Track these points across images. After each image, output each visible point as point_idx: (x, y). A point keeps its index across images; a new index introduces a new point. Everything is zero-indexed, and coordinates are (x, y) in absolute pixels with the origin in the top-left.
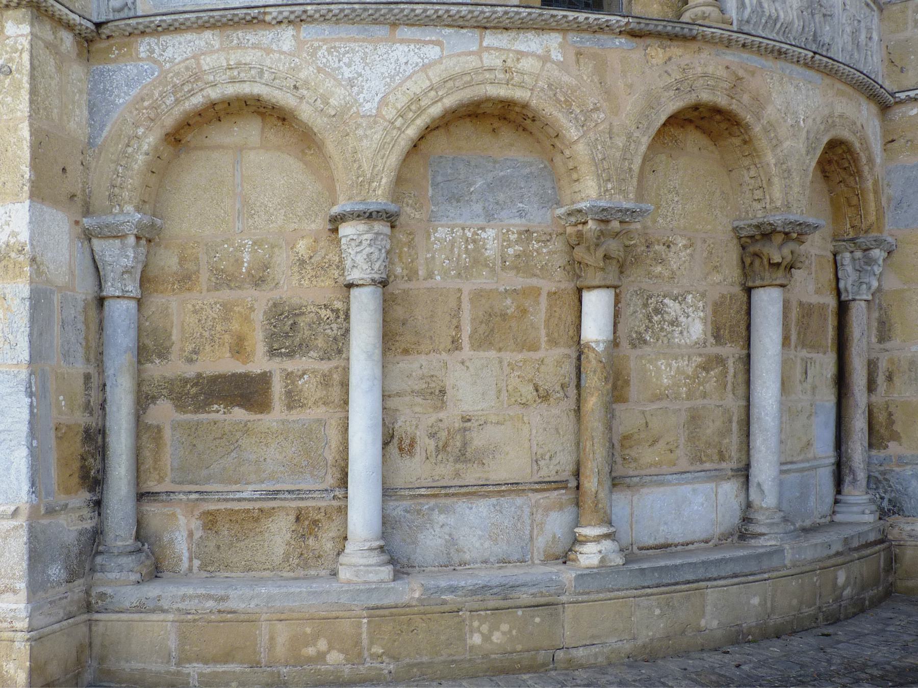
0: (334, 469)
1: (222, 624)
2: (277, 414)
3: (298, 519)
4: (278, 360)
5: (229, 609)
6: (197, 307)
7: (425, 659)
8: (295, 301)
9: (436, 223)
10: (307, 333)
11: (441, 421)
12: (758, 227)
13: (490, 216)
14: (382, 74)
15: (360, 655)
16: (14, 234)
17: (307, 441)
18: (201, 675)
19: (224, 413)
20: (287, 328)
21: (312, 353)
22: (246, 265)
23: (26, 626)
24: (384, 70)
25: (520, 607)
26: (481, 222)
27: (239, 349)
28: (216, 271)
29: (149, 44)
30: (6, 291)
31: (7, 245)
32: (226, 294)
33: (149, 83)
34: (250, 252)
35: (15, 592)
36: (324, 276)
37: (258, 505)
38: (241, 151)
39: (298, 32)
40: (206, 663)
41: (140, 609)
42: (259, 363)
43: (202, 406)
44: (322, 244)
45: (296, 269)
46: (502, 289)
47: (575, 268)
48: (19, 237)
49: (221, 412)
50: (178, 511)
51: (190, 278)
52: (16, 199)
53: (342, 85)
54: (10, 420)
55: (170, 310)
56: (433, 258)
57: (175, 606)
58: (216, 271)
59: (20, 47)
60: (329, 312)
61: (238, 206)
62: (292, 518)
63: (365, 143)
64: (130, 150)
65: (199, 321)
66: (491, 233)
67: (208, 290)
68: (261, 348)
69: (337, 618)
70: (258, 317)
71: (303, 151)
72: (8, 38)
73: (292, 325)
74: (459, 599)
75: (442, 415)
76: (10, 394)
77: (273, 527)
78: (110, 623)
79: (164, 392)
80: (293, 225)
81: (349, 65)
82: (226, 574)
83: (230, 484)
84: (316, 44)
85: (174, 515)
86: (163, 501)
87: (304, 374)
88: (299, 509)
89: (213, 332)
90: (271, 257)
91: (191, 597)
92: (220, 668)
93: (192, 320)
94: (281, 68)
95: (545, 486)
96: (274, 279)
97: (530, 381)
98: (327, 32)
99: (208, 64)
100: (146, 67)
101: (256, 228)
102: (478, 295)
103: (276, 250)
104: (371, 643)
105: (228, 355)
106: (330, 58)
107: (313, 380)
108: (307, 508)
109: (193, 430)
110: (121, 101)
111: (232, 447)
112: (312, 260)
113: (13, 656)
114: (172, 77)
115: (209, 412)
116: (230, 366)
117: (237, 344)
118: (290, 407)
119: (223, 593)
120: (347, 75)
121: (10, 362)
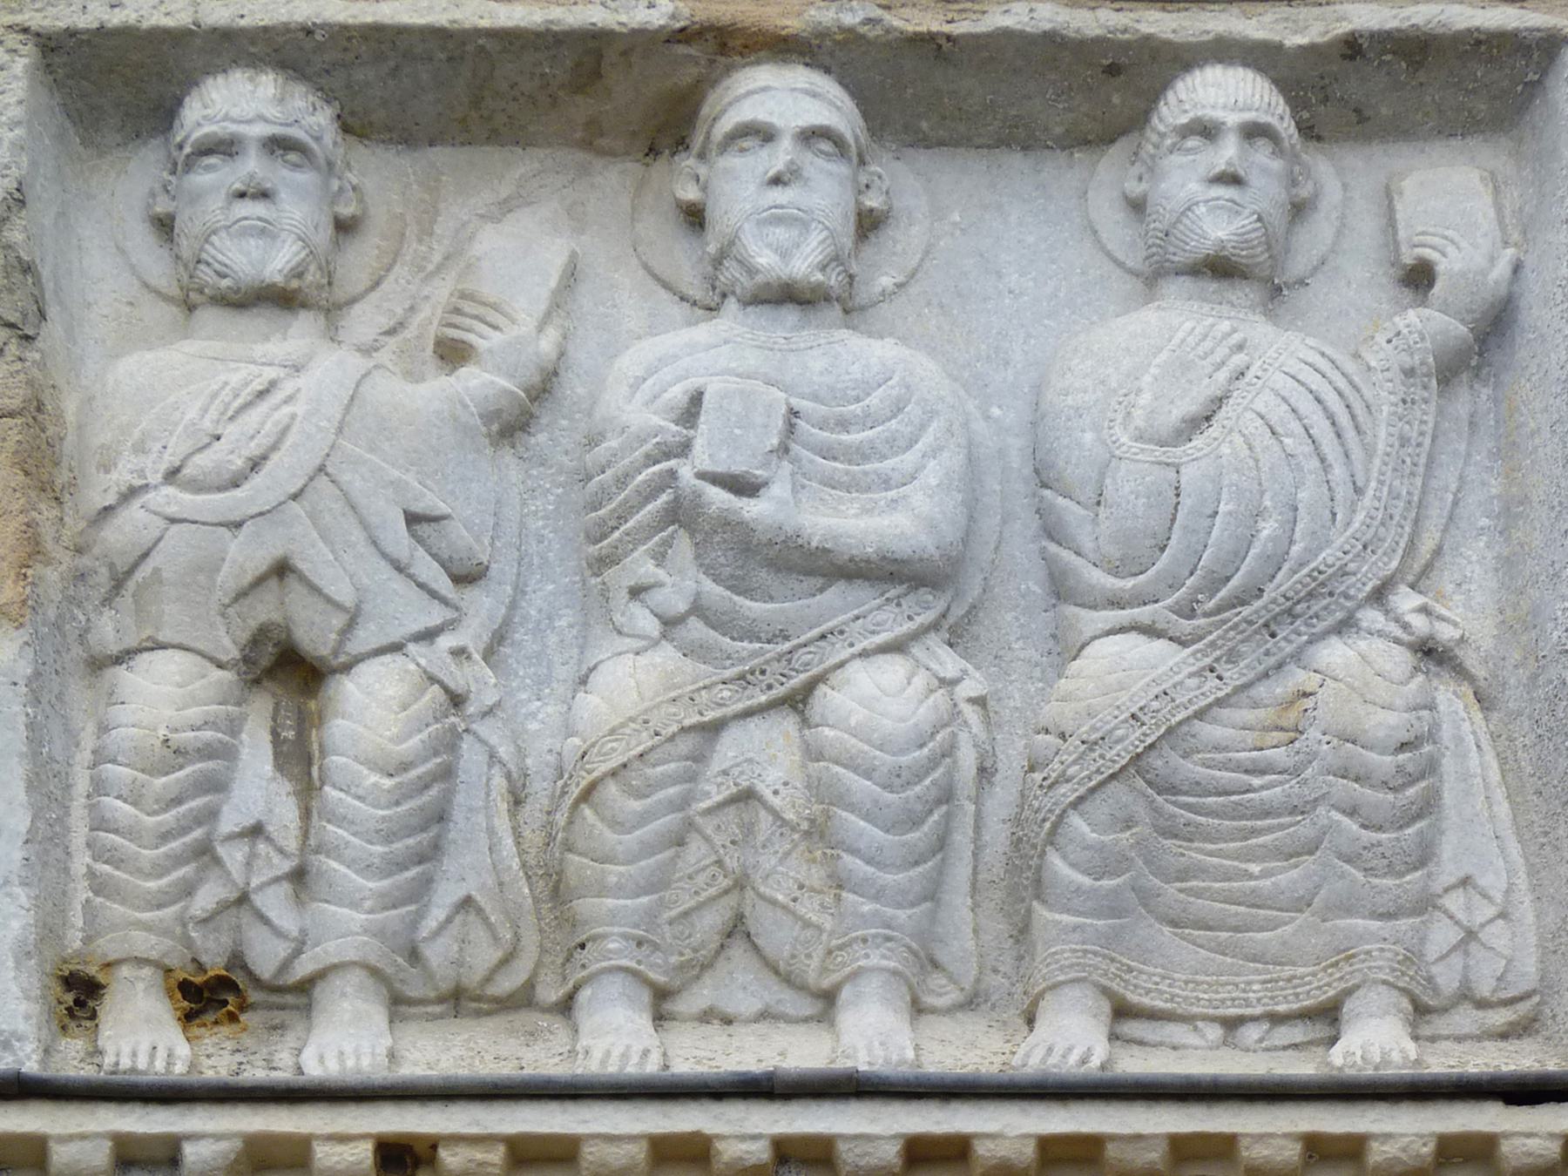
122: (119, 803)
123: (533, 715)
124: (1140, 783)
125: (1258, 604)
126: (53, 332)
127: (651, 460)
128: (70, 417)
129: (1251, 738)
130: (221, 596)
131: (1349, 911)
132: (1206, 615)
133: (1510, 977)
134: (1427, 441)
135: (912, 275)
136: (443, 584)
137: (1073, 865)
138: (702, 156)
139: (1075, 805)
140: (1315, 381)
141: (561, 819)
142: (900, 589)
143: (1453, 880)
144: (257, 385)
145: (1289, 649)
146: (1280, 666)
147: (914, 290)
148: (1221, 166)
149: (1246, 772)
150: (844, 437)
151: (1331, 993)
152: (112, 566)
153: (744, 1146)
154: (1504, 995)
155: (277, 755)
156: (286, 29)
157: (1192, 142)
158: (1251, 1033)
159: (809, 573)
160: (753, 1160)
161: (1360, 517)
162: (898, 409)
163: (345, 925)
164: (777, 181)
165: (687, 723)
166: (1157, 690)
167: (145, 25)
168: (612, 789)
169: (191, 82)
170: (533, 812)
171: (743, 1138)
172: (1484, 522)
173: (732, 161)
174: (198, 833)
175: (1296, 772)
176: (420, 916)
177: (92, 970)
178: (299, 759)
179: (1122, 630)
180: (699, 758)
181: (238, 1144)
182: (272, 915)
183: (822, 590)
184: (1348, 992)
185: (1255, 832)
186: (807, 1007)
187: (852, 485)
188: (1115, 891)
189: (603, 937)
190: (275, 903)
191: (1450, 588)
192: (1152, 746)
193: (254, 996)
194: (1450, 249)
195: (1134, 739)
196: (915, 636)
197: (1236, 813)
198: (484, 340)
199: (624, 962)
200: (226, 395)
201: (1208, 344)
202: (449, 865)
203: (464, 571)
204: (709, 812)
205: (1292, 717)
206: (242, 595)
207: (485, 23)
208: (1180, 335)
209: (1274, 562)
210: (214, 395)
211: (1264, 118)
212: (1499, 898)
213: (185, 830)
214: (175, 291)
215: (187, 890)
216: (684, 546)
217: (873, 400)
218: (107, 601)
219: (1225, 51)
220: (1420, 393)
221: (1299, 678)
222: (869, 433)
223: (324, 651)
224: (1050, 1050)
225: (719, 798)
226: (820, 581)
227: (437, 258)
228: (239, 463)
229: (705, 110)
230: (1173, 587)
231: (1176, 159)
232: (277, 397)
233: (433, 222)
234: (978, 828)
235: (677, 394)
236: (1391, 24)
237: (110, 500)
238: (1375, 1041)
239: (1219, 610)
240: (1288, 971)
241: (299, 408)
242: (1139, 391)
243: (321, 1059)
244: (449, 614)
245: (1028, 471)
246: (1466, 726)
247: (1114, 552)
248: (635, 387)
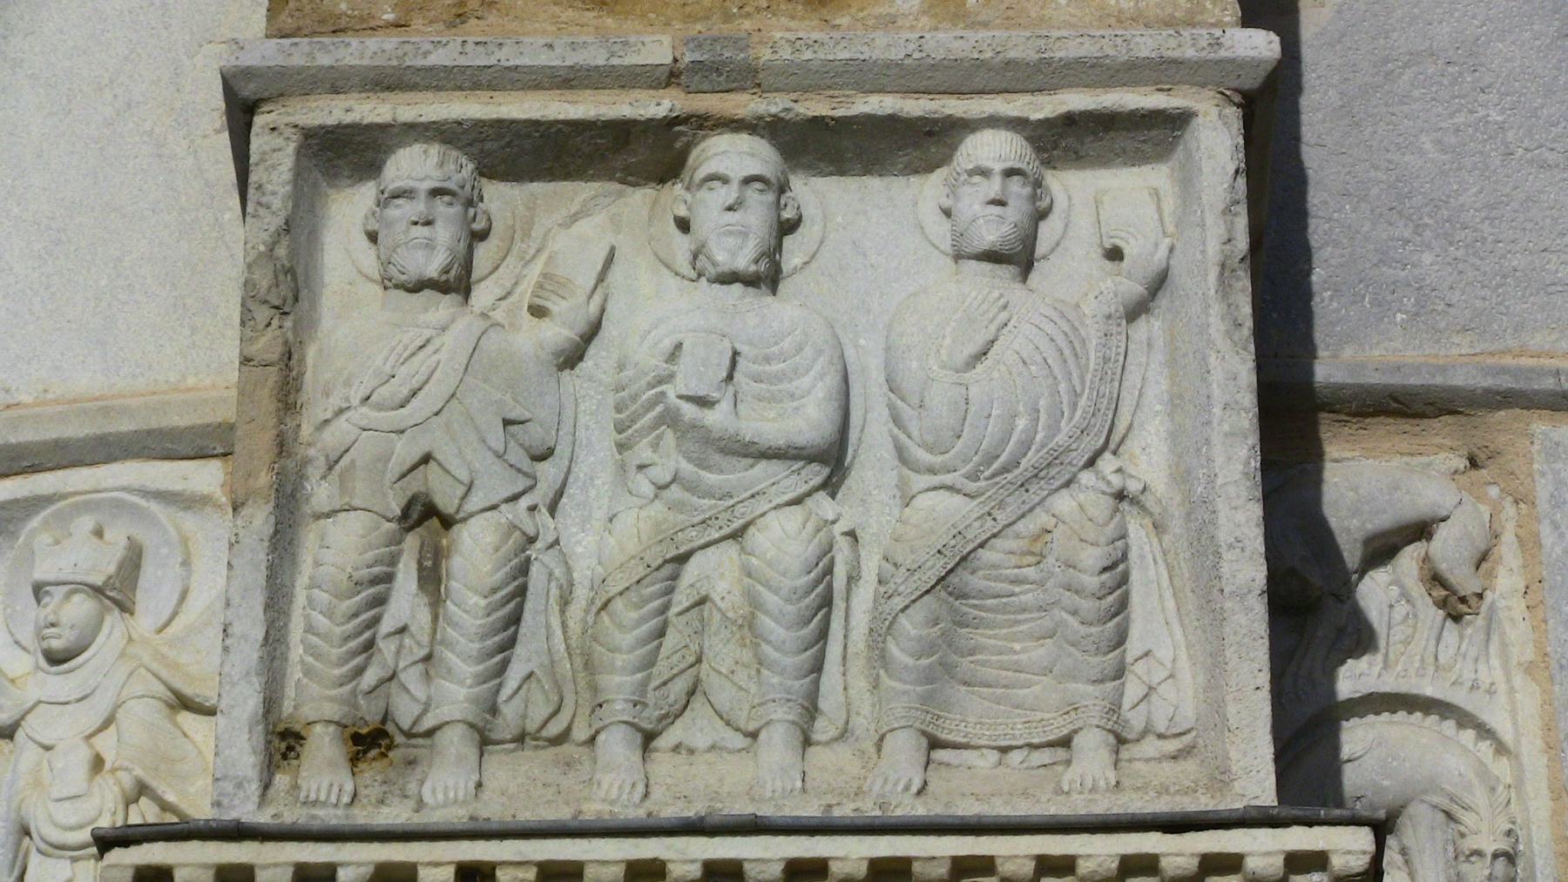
122: (320, 617)
123: (579, 542)
124: (943, 594)
125: (1017, 472)
126: (304, 304)
127: (651, 386)
128: (310, 360)
129: (1014, 560)
130: (391, 475)
131: (1075, 679)
132: (987, 479)
133: (1177, 719)
134: (1122, 358)
135: (813, 256)
136: (525, 463)
137: (902, 650)
138: (688, 189)
139: (902, 611)
140: (1049, 328)
141: (590, 619)
142: (801, 464)
143: (1140, 653)
144: (418, 343)
145: (1037, 499)
146: (1031, 510)
147: (814, 265)
148: (992, 195)
149: (1012, 582)
150: (767, 368)
151: (1065, 732)
152: (327, 457)
153: (686, 867)
154: (1175, 731)
155: (420, 579)
156: (446, 122)
157: (977, 179)
158: (1015, 757)
159: (745, 456)
160: (691, 877)
161: (1079, 413)
162: (800, 349)
163: (454, 696)
164: (730, 209)
165: (668, 556)
166: (955, 532)
167: (365, 122)
168: (618, 604)
169: (390, 150)
170: (576, 611)
171: (685, 862)
172: (1158, 407)
173: (703, 194)
174: (367, 635)
175: (1041, 584)
176: (500, 686)
177: (297, 728)
178: (432, 579)
179: (935, 488)
180: (675, 577)
181: (371, 869)
182: (411, 687)
183: (752, 466)
184: (1075, 732)
185: (1017, 622)
186: (739, 741)
187: (773, 399)
188: (930, 666)
189: (613, 701)
190: (411, 677)
191: (1138, 451)
192: (951, 571)
193: (399, 739)
194: (1131, 240)
195: (937, 568)
196: (809, 494)
197: (1003, 609)
198: (556, 306)
199: (625, 718)
200: (400, 348)
201: (985, 306)
202: (519, 650)
203: (538, 453)
204: (680, 614)
205: (1037, 548)
206: (404, 476)
207: (561, 117)
208: (969, 300)
209: (1026, 446)
210: (393, 349)
211: (1017, 165)
212: (1169, 666)
213: (360, 633)
214: (377, 277)
215: (359, 671)
216: (669, 437)
217: (786, 344)
218: (324, 477)
219: (994, 122)
220: (1114, 329)
221: (1041, 519)
222: (782, 365)
223: (451, 511)
224: (886, 780)
225: (686, 604)
226: (750, 461)
227: (532, 251)
228: (405, 392)
229: (691, 161)
230: (965, 462)
231: (967, 189)
232: (430, 348)
233: (530, 230)
234: (847, 619)
235: (667, 344)
236: (1091, 107)
237: (328, 415)
238: (1088, 782)
239: (993, 476)
240: (1039, 715)
241: (442, 356)
242: (944, 337)
243: (434, 791)
244: (529, 482)
245: (882, 380)
246: (1147, 548)
247: (930, 439)
248: (643, 338)
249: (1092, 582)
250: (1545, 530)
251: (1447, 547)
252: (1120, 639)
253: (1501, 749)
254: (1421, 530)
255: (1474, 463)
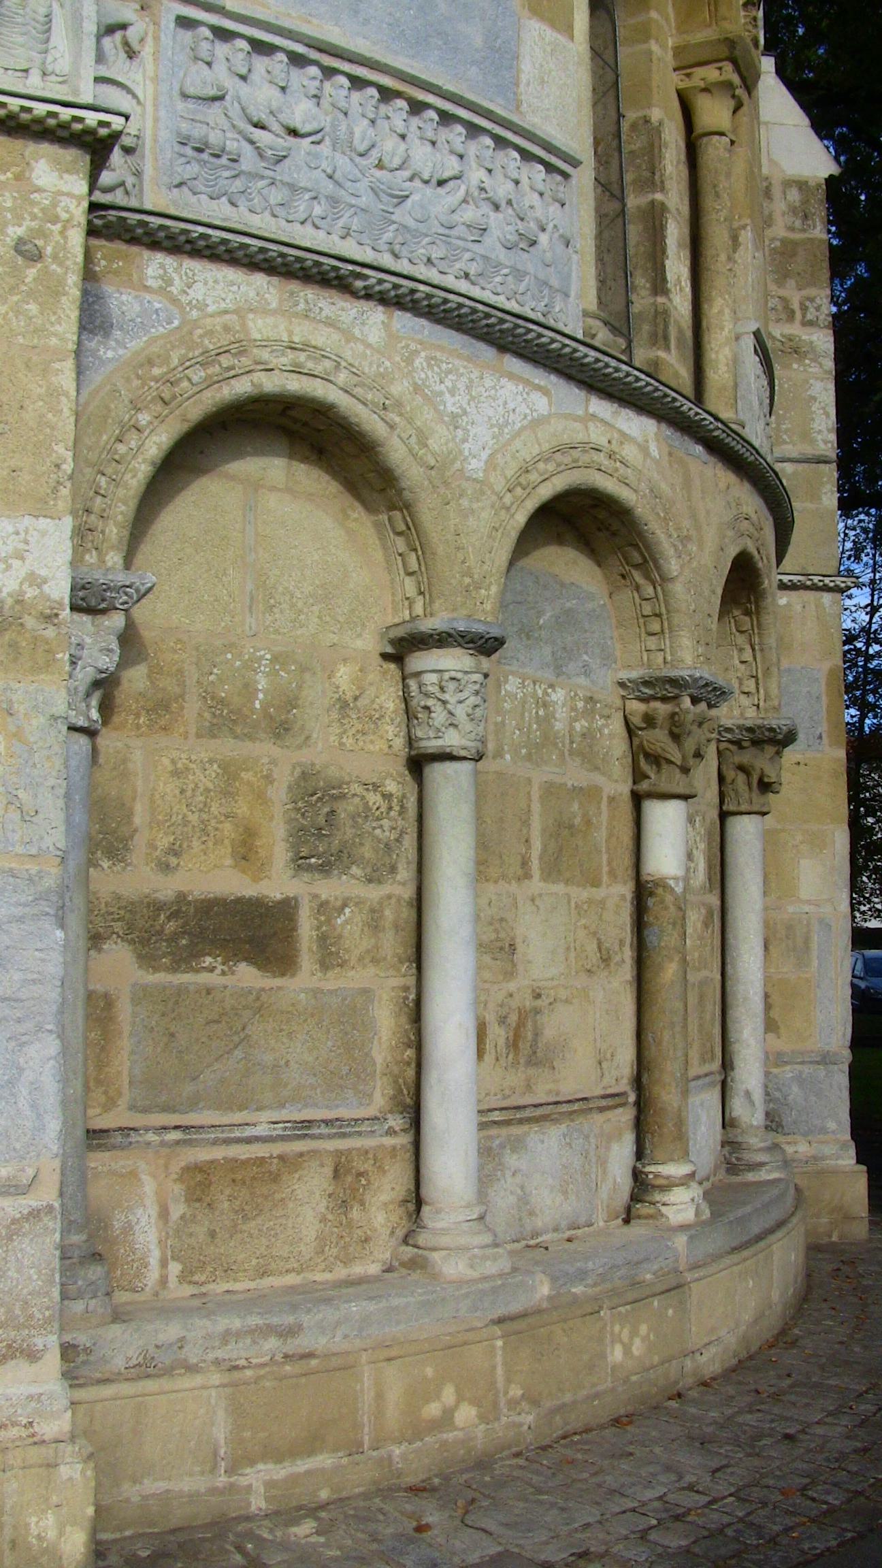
0: (385, 1079)
1: (303, 1380)
2: (307, 977)
3: (337, 1174)
4: (306, 877)
5: (301, 1351)
6: (179, 765)
7: (568, 1398)
8: (333, 772)
9: (507, 667)
10: (350, 832)
11: (511, 995)
12: (750, 730)
13: (559, 670)
14: (490, 418)
15: (495, 1404)
16: (33, 579)
17: (349, 1029)
18: (270, 1485)
19: (223, 973)
20: (321, 820)
21: (355, 870)
22: (261, 696)
23: (67, 1427)
24: (491, 412)
25: (654, 1295)
26: (549, 675)
27: (246, 853)
28: (213, 702)
29: (162, 266)
30: (15, 698)
31: (18, 602)
32: (227, 747)
33: (162, 336)
34: (267, 675)
35: (33, 1356)
36: (374, 733)
37: (277, 1149)
38: (256, 490)
39: (390, 317)
40: (279, 1459)
41: (145, 1369)
42: (278, 883)
43: (185, 960)
44: (371, 677)
45: (335, 715)
46: (570, 784)
47: (643, 759)
48: (46, 588)
49: (218, 971)
50: (142, 1165)
51: (167, 708)
52: (42, 509)
53: (443, 422)
54: (17, 976)
55: (130, 765)
56: (503, 723)
57: (211, 1356)
58: (213, 702)
59: (64, 216)
60: (379, 798)
61: (250, 586)
62: (328, 1171)
63: (471, 521)
64: (122, 448)
65: (182, 792)
66: (558, 696)
67: (199, 736)
68: (281, 854)
69: (465, 1343)
70: (279, 793)
71: (343, 511)
72: (39, 190)
73: (327, 814)
74: (590, 1291)
75: (512, 986)
76: (21, 919)
77: (301, 1190)
78: (99, 1407)
79: (118, 927)
80: (332, 636)
81: (452, 392)
82: (226, 1286)
83: (232, 1110)
84: (413, 346)
85: (134, 1174)
86: (114, 1147)
87: (345, 905)
88: (339, 1153)
89: (205, 816)
90: (300, 687)
91: (238, 1335)
92: (303, 1466)
93: (169, 788)
94: (366, 370)
95: (610, 1102)
96: (303, 728)
97: (595, 934)
98: (426, 332)
99: (260, 331)
100: (157, 305)
101: (277, 632)
102: (550, 790)
103: (307, 676)
104: (509, 1381)
105: (228, 861)
106: (430, 373)
107: (358, 919)
108: (349, 1151)
109: (170, 1004)
110: (110, 354)
111: (236, 1039)
112: (358, 703)
113: (55, 1499)
114: (201, 336)
115: (197, 971)
116: (229, 882)
117: (244, 843)
118: (325, 966)
119: (290, 1319)
120: (450, 408)
121: (20, 849)
158: (10, 72)
249: (42, 19)
250: (162, 35)
251: (132, 33)
252: (47, 41)
253: (139, 102)
254: (124, 27)
255: (142, 8)
